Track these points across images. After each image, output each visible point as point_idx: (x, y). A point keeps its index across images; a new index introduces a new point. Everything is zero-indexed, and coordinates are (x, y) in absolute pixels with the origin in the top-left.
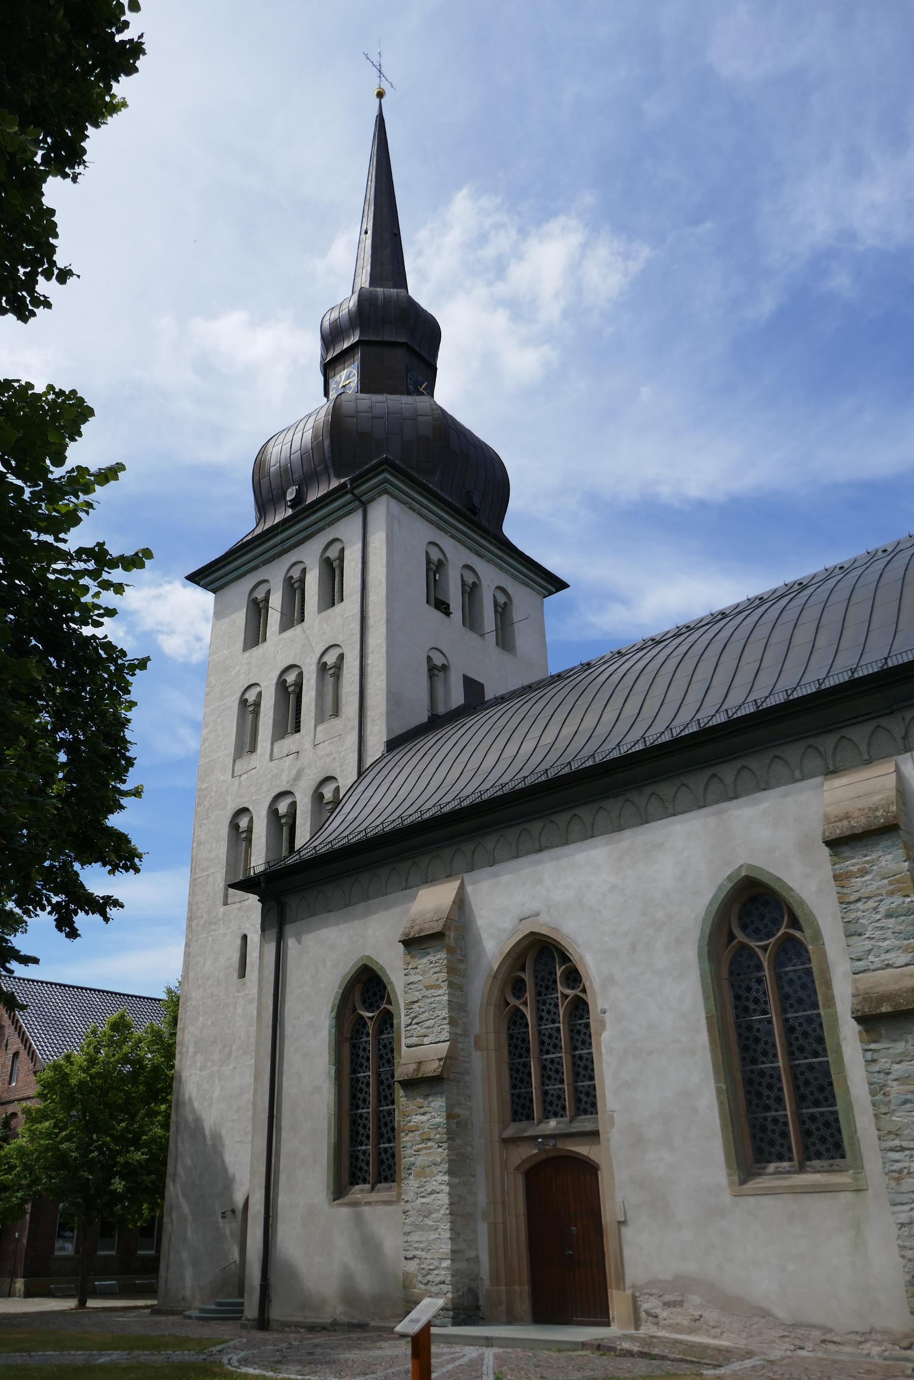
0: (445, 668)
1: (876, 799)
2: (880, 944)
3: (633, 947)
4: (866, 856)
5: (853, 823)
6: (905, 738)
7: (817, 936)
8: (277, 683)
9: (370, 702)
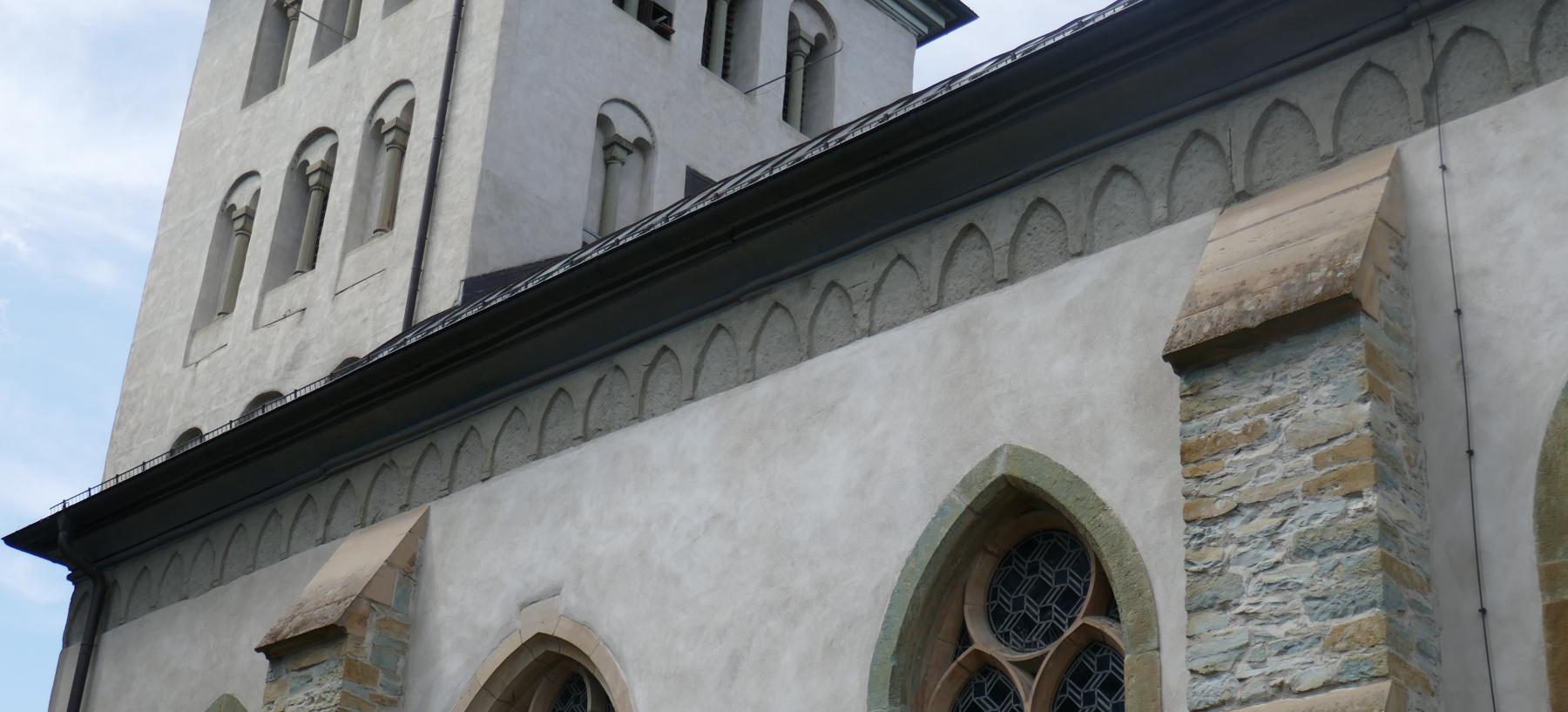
0: (643, 147)
1: (1321, 242)
2: (1272, 630)
3: (735, 661)
4: (1268, 391)
5: (1249, 305)
6: (1430, 89)
7: (1148, 626)
8: (291, 169)
9: (445, 198)
